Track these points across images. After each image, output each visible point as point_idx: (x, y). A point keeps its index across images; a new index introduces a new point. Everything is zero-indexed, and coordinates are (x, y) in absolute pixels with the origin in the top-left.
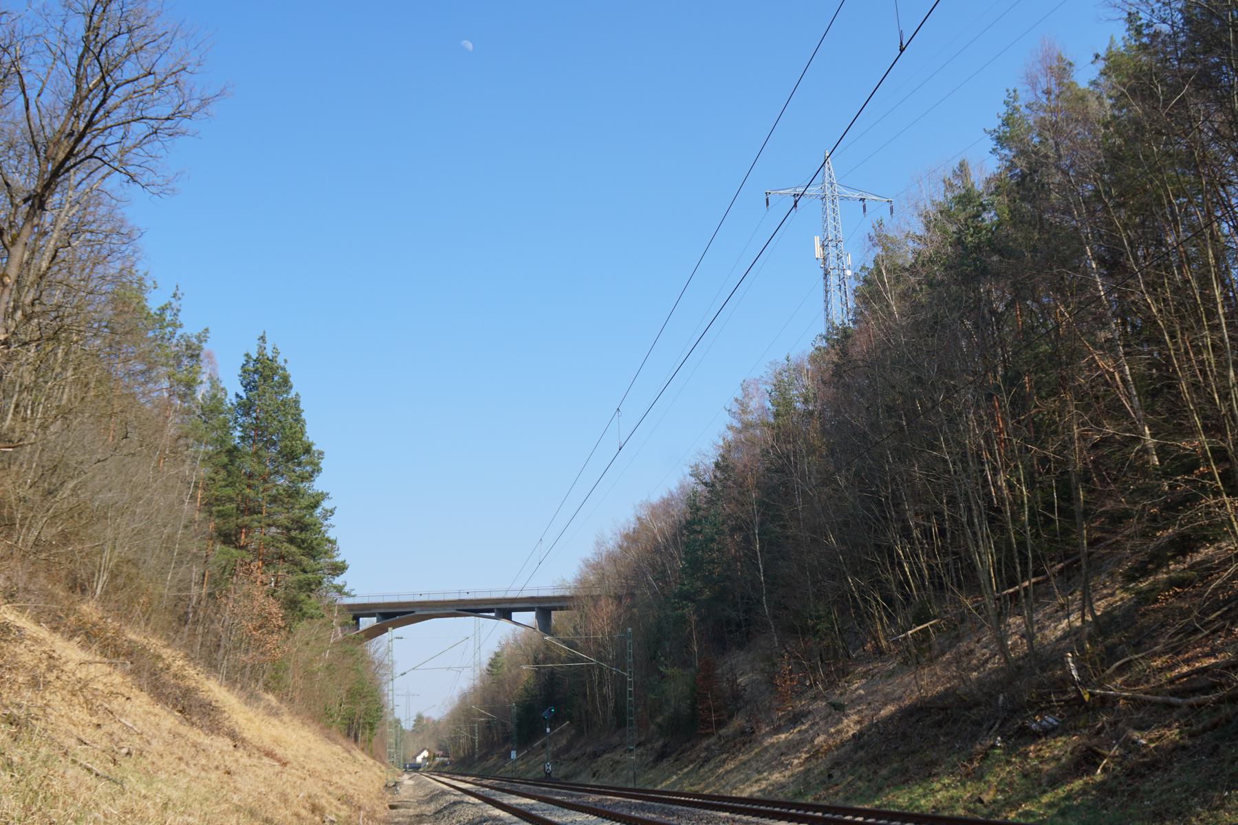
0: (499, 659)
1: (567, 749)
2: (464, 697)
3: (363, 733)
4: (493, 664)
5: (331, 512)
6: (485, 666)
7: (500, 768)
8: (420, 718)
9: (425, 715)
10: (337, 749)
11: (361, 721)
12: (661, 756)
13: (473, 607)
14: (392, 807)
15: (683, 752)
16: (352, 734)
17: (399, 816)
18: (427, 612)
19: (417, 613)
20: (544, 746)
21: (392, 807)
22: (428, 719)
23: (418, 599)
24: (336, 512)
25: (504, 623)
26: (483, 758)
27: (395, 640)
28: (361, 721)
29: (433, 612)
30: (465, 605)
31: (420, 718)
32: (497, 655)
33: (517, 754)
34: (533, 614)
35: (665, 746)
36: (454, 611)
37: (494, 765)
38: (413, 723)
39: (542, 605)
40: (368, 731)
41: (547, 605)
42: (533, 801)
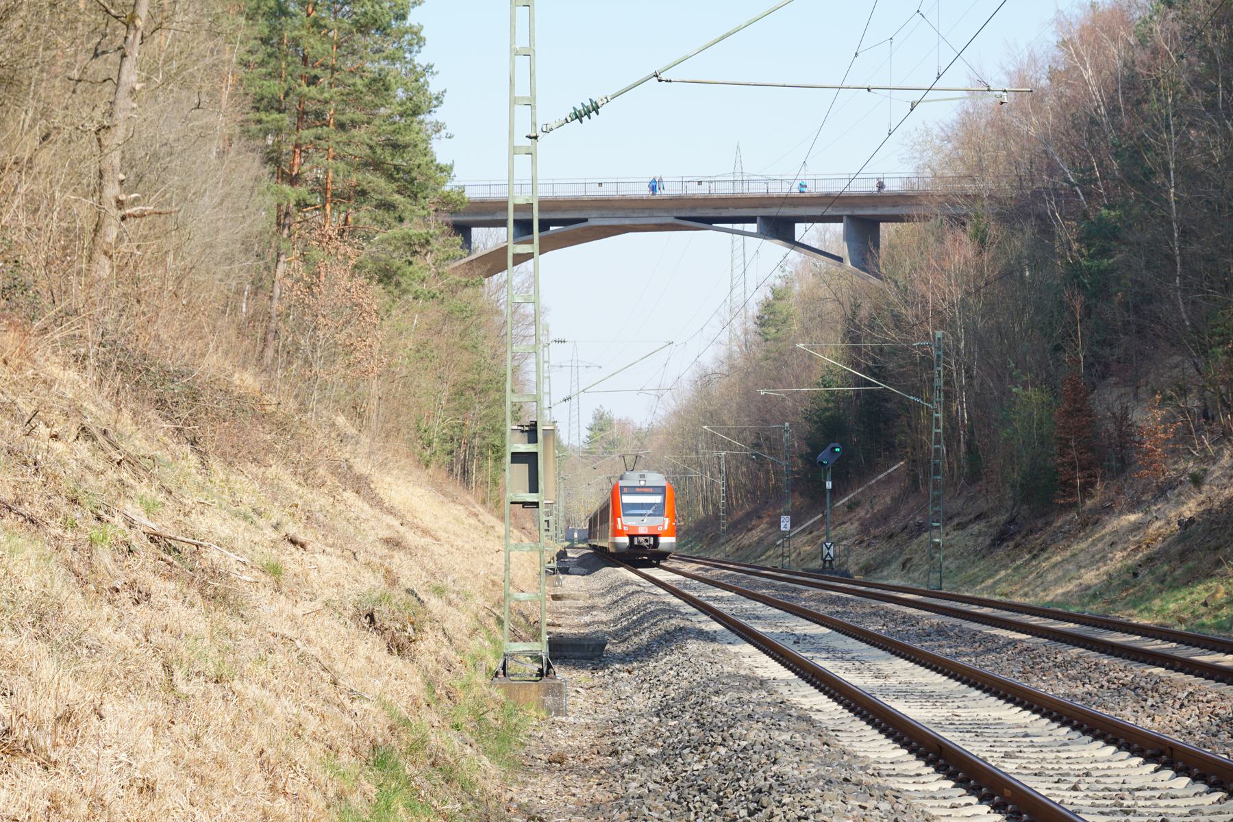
0: (780, 305)
1: (884, 517)
2: (705, 382)
3: (480, 468)
4: (588, 574)
5: (437, 98)
6: (754, 310)
7: (768, 549)
8: (601, 424)
9: (617, 414)
10: (458, 510)
11: (477, 441)
12: (1001, 538)
13: (711, 213)
14: (556, 597)
15: (1031, 532)
16: (458, 469)
17: (565, 607)
18: (614, 222)
19: (593, 222)
20: (852, 507)
21: (556, 597)
22: (623, 424)
23: (594, 192)
24: (445, 100)
25: (775, 249)
26: (739, 526)
27: (553, 345)
28: (477, 441)
29: (627, 222)
30: (694, 208)
31: (601, 424)
32: (778, 295)
33: (794, 524)
34: (839, 228)
35: (1012, 521)
36: (670, 220)
37: (761, 540)
38: (585, 433)
39: (858, 212)
40: (490, 463)
41: (869, 212)
42: (731, 594)
